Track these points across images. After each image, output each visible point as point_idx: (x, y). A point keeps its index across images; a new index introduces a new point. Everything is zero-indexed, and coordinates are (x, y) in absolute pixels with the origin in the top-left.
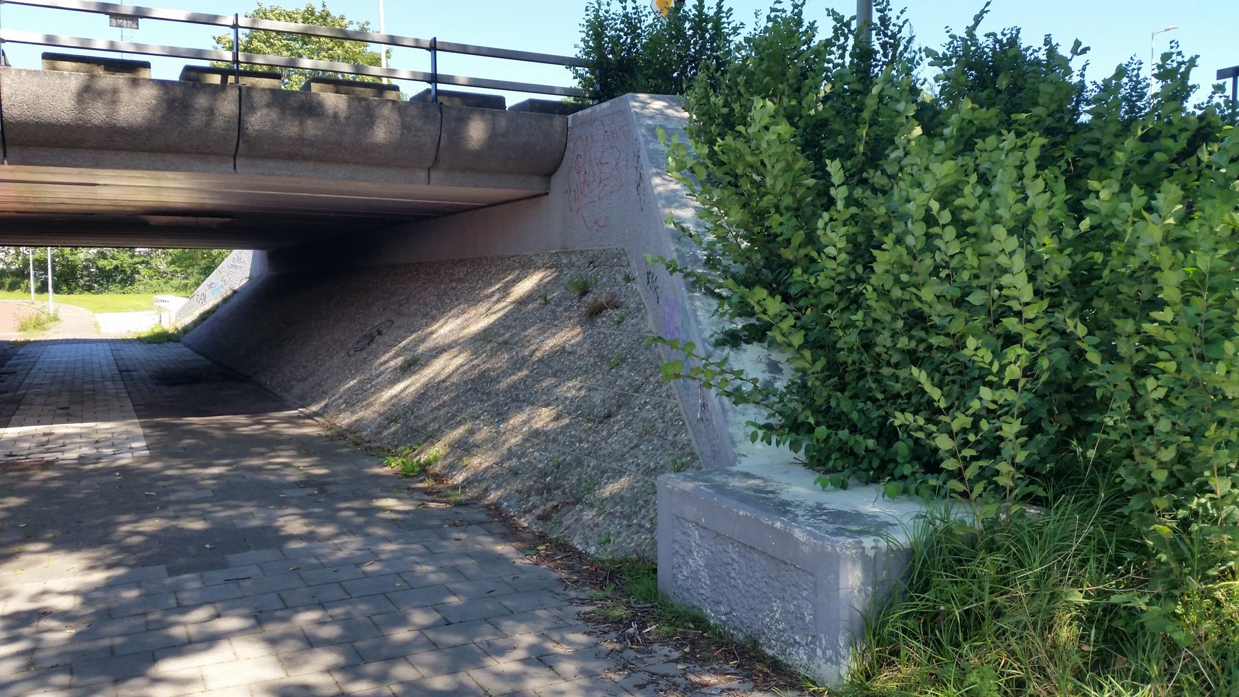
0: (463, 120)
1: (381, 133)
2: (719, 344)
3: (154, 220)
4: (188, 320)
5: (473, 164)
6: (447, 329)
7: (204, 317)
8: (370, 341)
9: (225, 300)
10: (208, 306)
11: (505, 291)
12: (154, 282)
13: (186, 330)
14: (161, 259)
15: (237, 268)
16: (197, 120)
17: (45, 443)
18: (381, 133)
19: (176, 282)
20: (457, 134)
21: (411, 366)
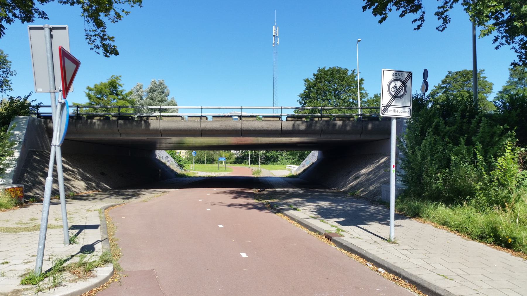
0: (367, 123)
1: (348, 128)
2: (401, 169)
3: (299, 145)
4: (300, 172)
5: (371, 132)
6: (364, 171)
7: (305, 171)
8: (349, 174)
9: (311, 166)
10: (306, 167)
11: (379, 161)
12: (283, 161)
13: (300, 174)
14: (285, 154)
15: (313, 157)
16: (313, 128)
17: (288, 191)
18: (348, 128)
19: (290, 161)
20: (366, 127)
21: (356, 178)
